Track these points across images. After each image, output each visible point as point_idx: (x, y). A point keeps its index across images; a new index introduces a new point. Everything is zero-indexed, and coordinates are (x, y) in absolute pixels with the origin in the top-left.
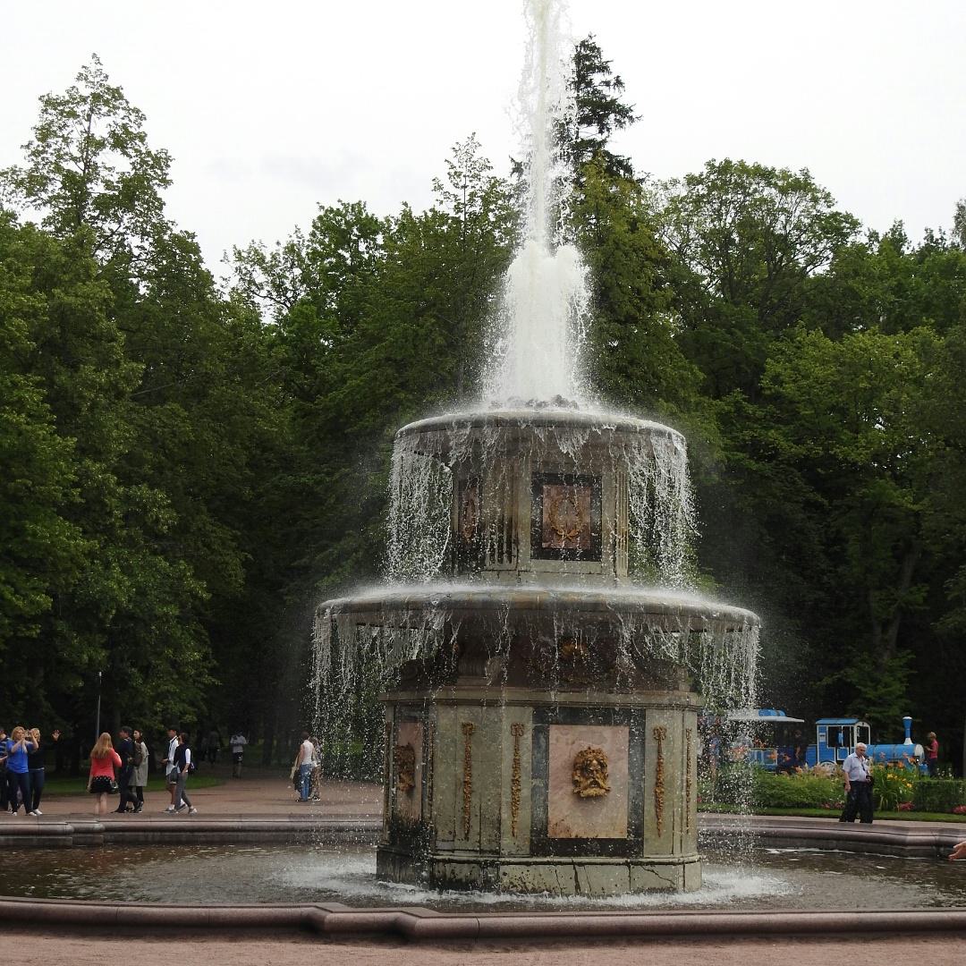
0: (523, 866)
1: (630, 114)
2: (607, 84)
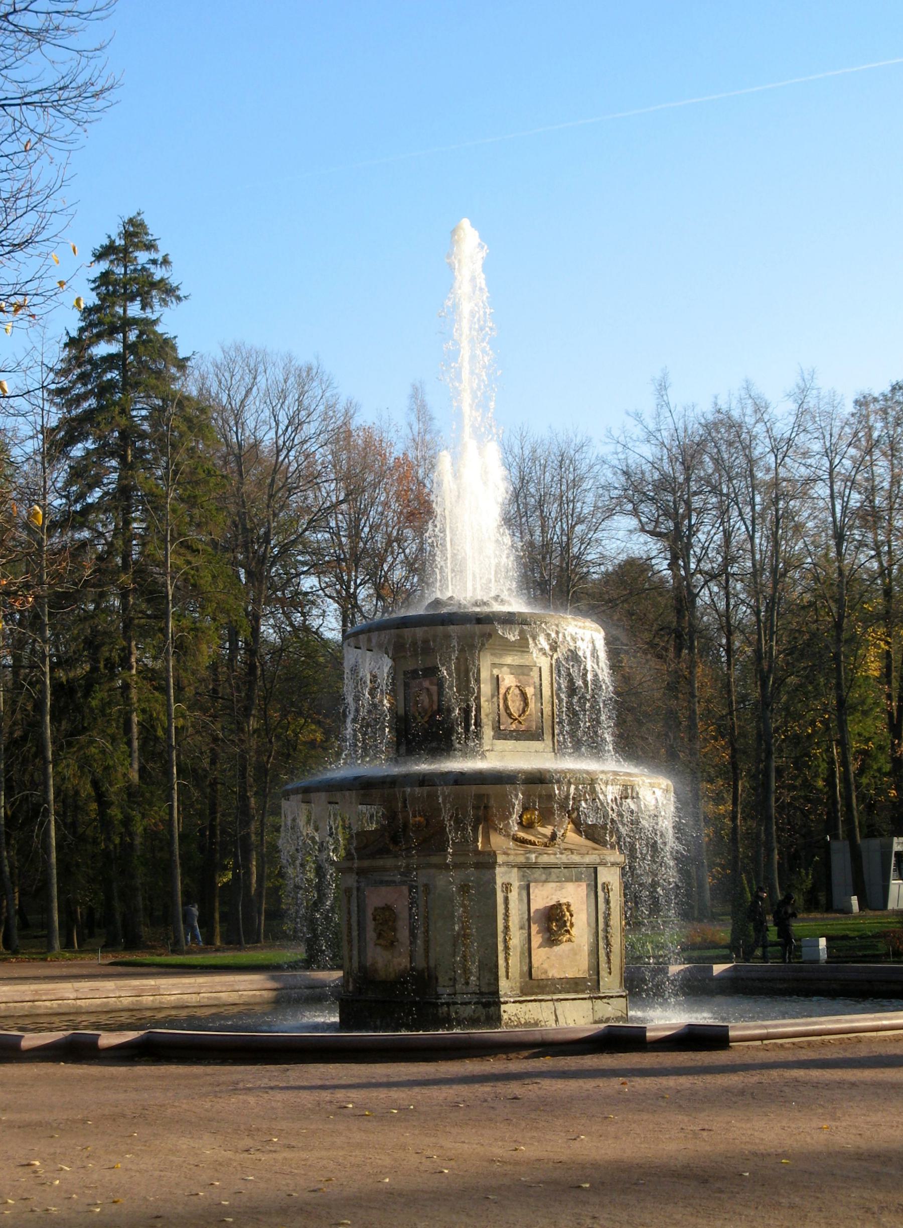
0: (517, 1004)
1: (178, 293)
2: (154, 262)
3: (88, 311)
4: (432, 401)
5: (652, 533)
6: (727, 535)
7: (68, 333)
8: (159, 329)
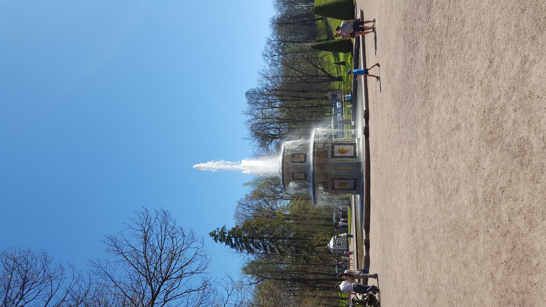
3: (226, 244)
4: (246, 182)
5: (272, 142)
6: (273, 128)
7: (230, 248)
8: (230, 230)
